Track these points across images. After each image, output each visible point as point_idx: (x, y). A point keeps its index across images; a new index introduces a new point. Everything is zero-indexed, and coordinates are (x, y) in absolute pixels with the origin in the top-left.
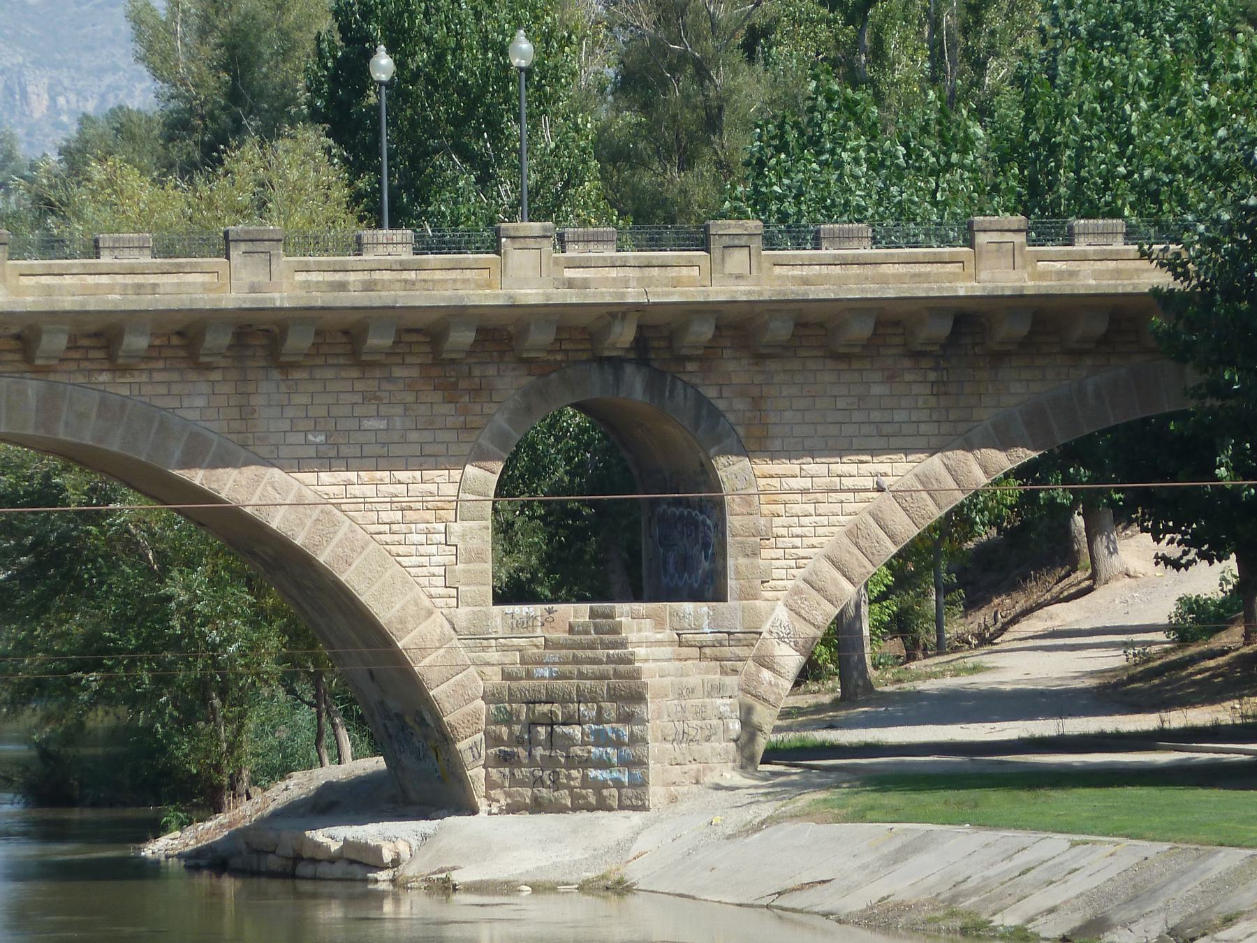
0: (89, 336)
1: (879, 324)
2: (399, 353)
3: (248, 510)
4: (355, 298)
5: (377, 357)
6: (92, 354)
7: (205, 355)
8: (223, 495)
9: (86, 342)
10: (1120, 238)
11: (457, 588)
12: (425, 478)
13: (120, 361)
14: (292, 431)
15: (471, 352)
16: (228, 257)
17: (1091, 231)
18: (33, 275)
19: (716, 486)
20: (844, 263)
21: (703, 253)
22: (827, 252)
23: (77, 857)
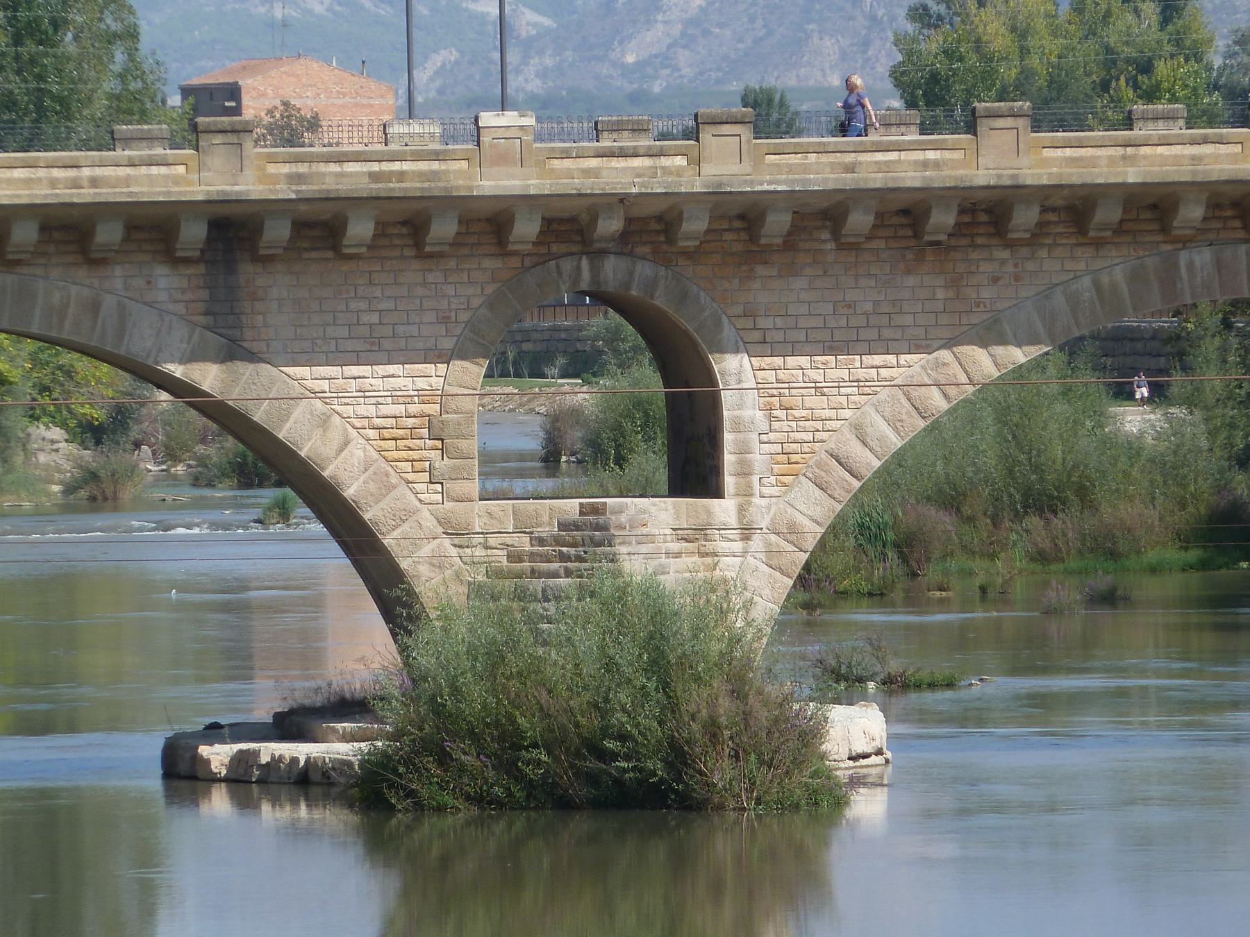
0: (395, 224)
1: (548, 222)
2: (1214, 229)
3: (230, 403)
4: (86, 195)
5: (22, 256)
6: (901, 233)
7: (13, 252)
8: (205, 387)
9: (897, 220)
10: (1181, 122)
11: (442, 484)
12: (902, 362)
13: (428, 249)
14: (874, 313)
15: (456, 244)
16: (698, 140)
17: (1150, 117)
18: (1081, 147)
19: (712, 381)
20: (132, 164)
21: (692, 142)
22: (121, 153)
23: (1090, 719)
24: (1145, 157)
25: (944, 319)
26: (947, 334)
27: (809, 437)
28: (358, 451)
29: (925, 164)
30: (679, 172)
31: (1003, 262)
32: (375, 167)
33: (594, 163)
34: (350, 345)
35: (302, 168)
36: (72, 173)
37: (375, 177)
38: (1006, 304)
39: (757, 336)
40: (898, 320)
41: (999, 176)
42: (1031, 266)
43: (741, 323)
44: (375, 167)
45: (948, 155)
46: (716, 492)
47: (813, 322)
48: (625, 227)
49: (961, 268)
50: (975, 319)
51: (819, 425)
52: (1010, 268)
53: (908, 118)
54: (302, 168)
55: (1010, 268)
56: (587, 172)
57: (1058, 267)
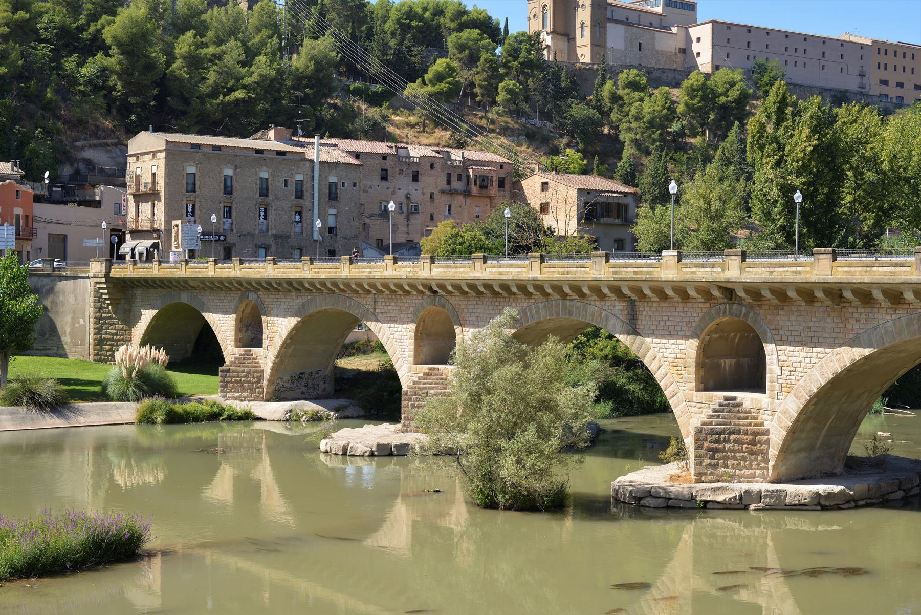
24: (874, 272)
25: (841, 335)
26: (842, 342)
27: (793, 378)
28: (662, 371)
29: (795, 273)
30: (718, 273)
31: (861, 314)
32: (636, 269)
33: (694, 269)
34: (662, 332)
35: (617, 269)
36: (563, 270)
37: (635, 273)
38: (862, 331)
39: (778, 338)
40: (825, 335)
41: (819, 278)
42: (871, 316)
43: (774, 332)
44: (636, 269)
45: (804, 269)
46: (764, 392)
47: (796, 334)
48: (55, 285)
49: (847, 315)
50: (851, 336)
51: (796, 374)
52: (863, 316)
53: (11, 236)
54: (617, 269)
55: (863, 316)
56: (692, 273)
57: (881, 317)
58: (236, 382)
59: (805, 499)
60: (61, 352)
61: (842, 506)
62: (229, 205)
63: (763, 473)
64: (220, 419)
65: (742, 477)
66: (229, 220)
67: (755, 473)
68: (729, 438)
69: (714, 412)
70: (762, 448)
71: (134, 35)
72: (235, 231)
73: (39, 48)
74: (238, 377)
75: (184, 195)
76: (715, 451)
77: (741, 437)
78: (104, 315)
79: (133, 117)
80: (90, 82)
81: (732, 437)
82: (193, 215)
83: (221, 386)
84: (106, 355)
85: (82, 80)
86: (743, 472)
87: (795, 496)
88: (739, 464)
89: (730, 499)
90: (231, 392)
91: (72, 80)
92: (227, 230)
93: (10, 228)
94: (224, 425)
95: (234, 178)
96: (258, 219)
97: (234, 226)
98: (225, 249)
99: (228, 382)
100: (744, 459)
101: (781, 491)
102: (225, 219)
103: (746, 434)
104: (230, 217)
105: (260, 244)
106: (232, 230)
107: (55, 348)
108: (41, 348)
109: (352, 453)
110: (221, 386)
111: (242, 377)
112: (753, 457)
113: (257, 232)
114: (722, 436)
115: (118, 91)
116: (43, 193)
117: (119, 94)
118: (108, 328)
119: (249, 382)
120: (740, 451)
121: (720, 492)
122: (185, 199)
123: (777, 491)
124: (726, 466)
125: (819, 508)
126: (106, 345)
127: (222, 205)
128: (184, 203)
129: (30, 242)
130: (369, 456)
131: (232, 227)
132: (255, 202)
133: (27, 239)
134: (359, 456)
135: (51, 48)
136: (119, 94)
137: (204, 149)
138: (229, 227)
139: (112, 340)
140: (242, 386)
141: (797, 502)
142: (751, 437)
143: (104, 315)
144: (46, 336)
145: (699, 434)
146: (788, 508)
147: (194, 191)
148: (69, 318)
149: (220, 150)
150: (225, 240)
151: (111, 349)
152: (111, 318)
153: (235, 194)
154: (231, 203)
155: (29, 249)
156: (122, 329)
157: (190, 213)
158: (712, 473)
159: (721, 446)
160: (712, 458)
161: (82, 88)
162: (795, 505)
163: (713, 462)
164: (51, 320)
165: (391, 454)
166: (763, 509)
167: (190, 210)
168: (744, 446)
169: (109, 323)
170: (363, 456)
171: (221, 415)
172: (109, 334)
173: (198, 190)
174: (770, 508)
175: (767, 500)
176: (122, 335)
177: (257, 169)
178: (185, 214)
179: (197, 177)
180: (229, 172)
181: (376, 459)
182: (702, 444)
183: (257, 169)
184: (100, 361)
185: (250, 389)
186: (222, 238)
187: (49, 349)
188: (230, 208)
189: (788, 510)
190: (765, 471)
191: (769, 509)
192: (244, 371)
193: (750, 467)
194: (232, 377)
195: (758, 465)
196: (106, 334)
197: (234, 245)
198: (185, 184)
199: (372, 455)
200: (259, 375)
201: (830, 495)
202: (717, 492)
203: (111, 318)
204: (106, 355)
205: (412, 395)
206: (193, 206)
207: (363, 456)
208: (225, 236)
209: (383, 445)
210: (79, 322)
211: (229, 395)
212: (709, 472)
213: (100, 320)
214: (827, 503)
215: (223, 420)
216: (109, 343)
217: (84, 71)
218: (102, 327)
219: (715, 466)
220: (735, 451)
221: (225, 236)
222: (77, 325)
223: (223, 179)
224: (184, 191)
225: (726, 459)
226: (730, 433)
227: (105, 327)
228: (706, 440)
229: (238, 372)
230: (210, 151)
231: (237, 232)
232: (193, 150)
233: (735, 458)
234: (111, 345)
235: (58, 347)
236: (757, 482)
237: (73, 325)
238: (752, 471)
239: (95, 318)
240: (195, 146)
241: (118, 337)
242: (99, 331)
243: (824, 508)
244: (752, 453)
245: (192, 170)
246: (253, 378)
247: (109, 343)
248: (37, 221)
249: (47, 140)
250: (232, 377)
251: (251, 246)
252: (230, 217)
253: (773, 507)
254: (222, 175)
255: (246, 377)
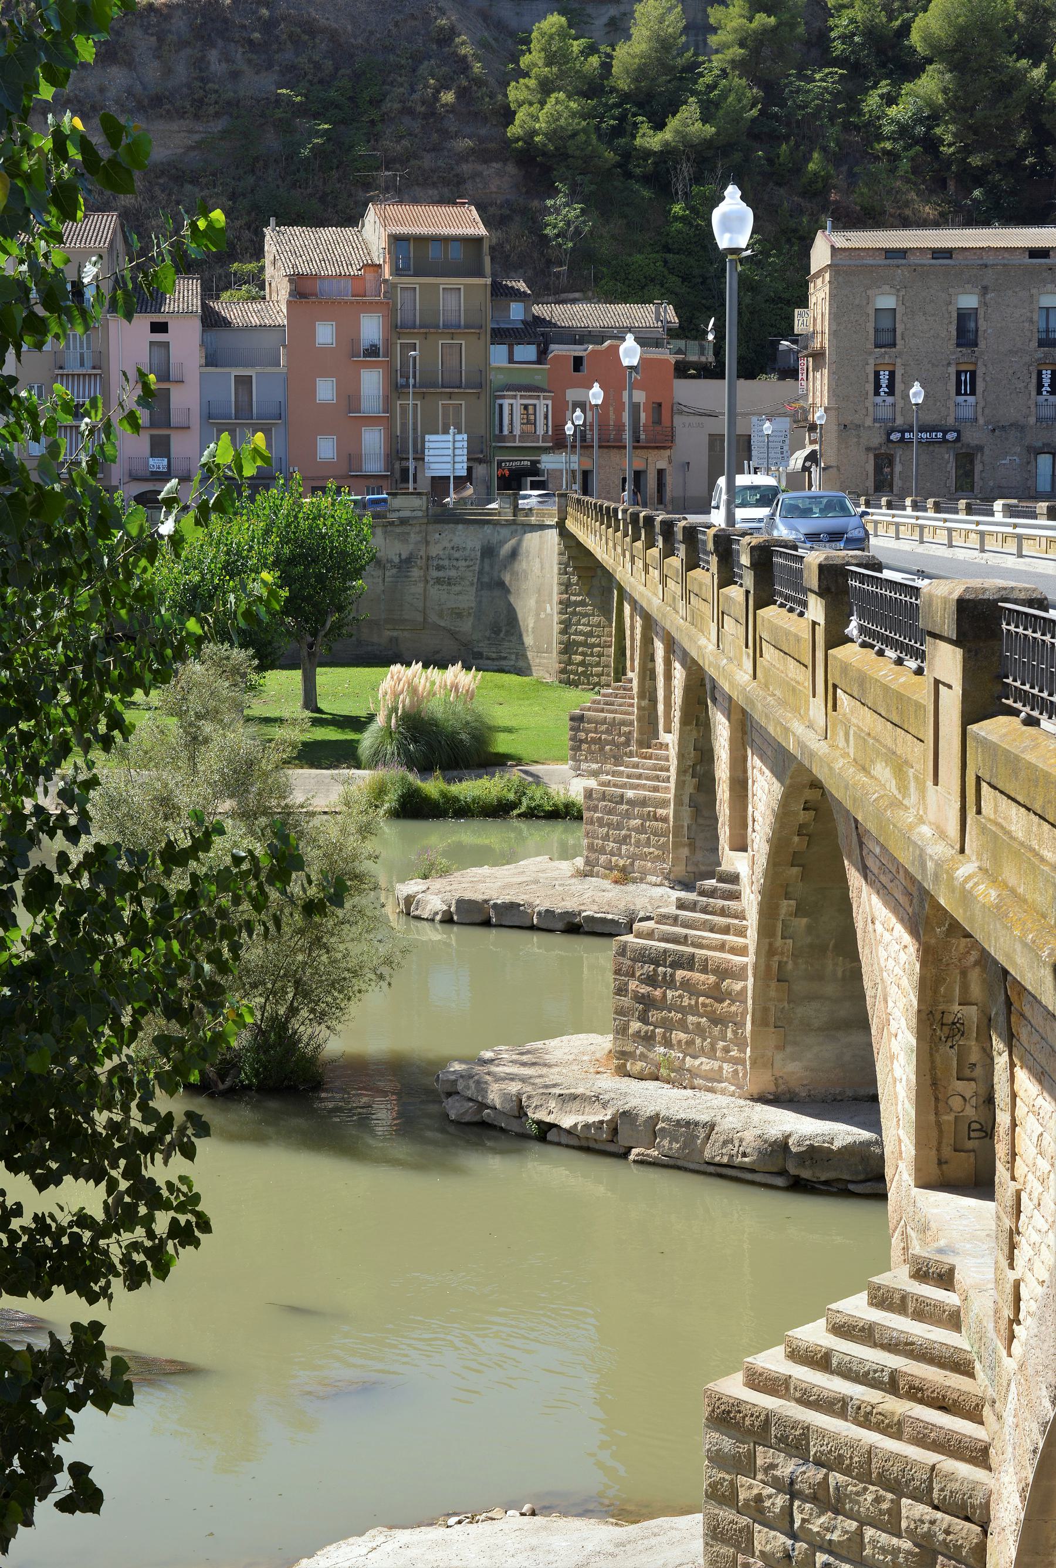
58: (594, 741)
59: (744, 1155)
60: (521, 664)
61: (851, 1187)
62: (971, 368)
63: (736, 1072)
64: (515, 812)
65: (697, 1076)
66: (971, 399)
67: (721, 1068)
68: (672, 975)
69: (679, 907)
70: (733, 1008)
71: (961, 29)
72: (981, 421)
73: (818, 76)
74: (596, 732)
75: (870, 353)
76: (647, 1003)
77: (697, 976)
78: (573, 598)
79: (977, 193)
80: (903, 130)
81: (680, 974)
82: (891, 392)
83: (572, 749)
84: (576, 673)
85: (887, 130)
86: (697, 1062)
87: (725, 1143)
88: (690, 1043)
89: (587, 1126)
90: (586, 760)
91: (871, 130)
92: (965, 420)
93: (459, 437)
94: (523, 825)
95: (981, 313)
96: (1034, 393)
97: (980, 410)
98: (957, 456)
99: (581, 741)
100: (700, 1030)
101: (697, 1124)
102: (961, 398)
103: (704, 970)
104: (973, 392)
105: (1039, 444)
106: (976, 420)
107: (513, 657)
108: (494, 655)
109: (416, 913)
110: (572, 749)
111: (602, 733)
112: (716, 1030)
113: (1032, 420)
114: (661, 969)
115: (950, 145)
116: (703, 359)
117: (952, 149)
118: (578, 623)
119: (612, 743)
120: (693, 1010)
121: (576, 1105)
122: (871, 361)
123: (688, 1123)
124: (668, 1043)
125: (780, 1181)
126: (576, 653)
127: (952, 370)
128: (870, 370)
129: (668, 452)
130: (442, 922)
131: (976, 412)
132: (1027, 359)
133: (657, 448)
134: (427, 919)
135: (841, 75)
136: (952, 149)
137: (912, 259)
138: (968, 413)
139: (585, 644)
140: (602, 749)
141: (725, 1160)
142: (712, 979)
143: (573, 598)
144: (502, 635)
145: (621, 959)
146: (711, 1169)
147: (894, 345)
148: (532, 602)
149: (951, 258)
150: (958, 439)
151: (583, 661)
152: (582, 603)
153: (982, 344)
154: (976, 364)
155: (662, 464)
156: (598, 625)
157: (884, 389)
158: (643, 1057)
159: (658, 993)
160: (644, 1019)
161: (888, 145)
162: (742, 1168)
163: (645, 1028)
164: (510, 604)
165: (487, 923)
166: (654, 1164)
167: (884, 382)
168: (701, 999)
169: (580, 614)
170: (433, 920)
171: (514, 805)
172: (581, 633)
173: (899, 341)
174: (672, 1162)
175: (666, 1143)
176: (598, 636)
177: (1034, 291)
178: (871, 392)
179: (898, 316)
180: (969, 301)
181: (455, 928)
182: (627, 984)
183: (1034, 291)
184: (569, 683)
185: (614, 757)
186: (951, 436)
187: (505, 658)
188: (973, 374)
189: (711, 1174)
190: (740, 1067)
191: (671, 1165)
192: (604, 721)
193: (712, 1054)
194: (587, 732)
195: (726, 1050)
196: (576, 633)
197: (980, 448)
198: (872, 332)
199: (448, 920)
200: (627, 729)
201: (815, 1154)
202: (569, 1106)
203: (582, 603)
204: (576, 673)
205: (599, 800)
206: (892, 374)
207: (433, 920)
208: (958, 432)
209: (471, 902)
210: (545, 610)
211: (584, 766)
212: (638, 1052)
213: (567, 606)
214: (806, 1174)
215: (519, 816)
216: (581, 649)
217: (893, 111)
218: (570, 620)
219: (648, 1039)
220: (681, 1009)
221: (958, 432)
222: (542, 616)
223: (955, 315)
224: (870, 345)
225: (668, 1026)
226: (676, 965)
227: (574, 619)
228: (633, 975)
229: (597, 723)
230: (927, 260)
231: (987, 423)
232: (889, 261)
233: (683, 1026)
234: (583, 654)
235: (517, 654)
236: (723, 1092)
237: (538, 615)
238: (716, 1064)
239: (561, 603)
240: (891, 253)
241: (593, 640)
242: (566, 627)
243: (798, 1186)
244: (716, 1020)
245: (887, 301)
246: (620, 735)
247: (581, 649)
248: (681, 413)
249: (770, 256)
250: (587, 732)
251: (1018, 449)
252: (973, 392)
253: (680, 1163)
254: (953, 309)
255: (608, 732)
